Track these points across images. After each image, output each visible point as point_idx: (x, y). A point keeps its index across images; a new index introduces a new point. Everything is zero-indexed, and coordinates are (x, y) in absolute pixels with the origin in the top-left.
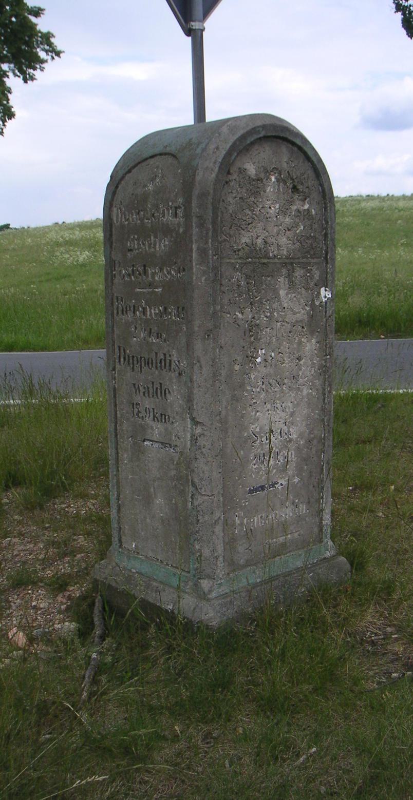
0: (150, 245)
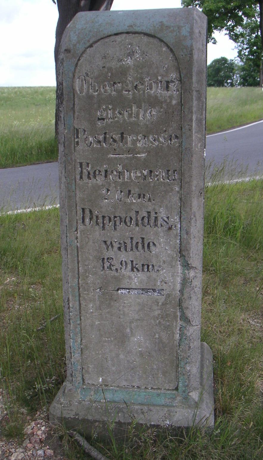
0: (130, 115)
